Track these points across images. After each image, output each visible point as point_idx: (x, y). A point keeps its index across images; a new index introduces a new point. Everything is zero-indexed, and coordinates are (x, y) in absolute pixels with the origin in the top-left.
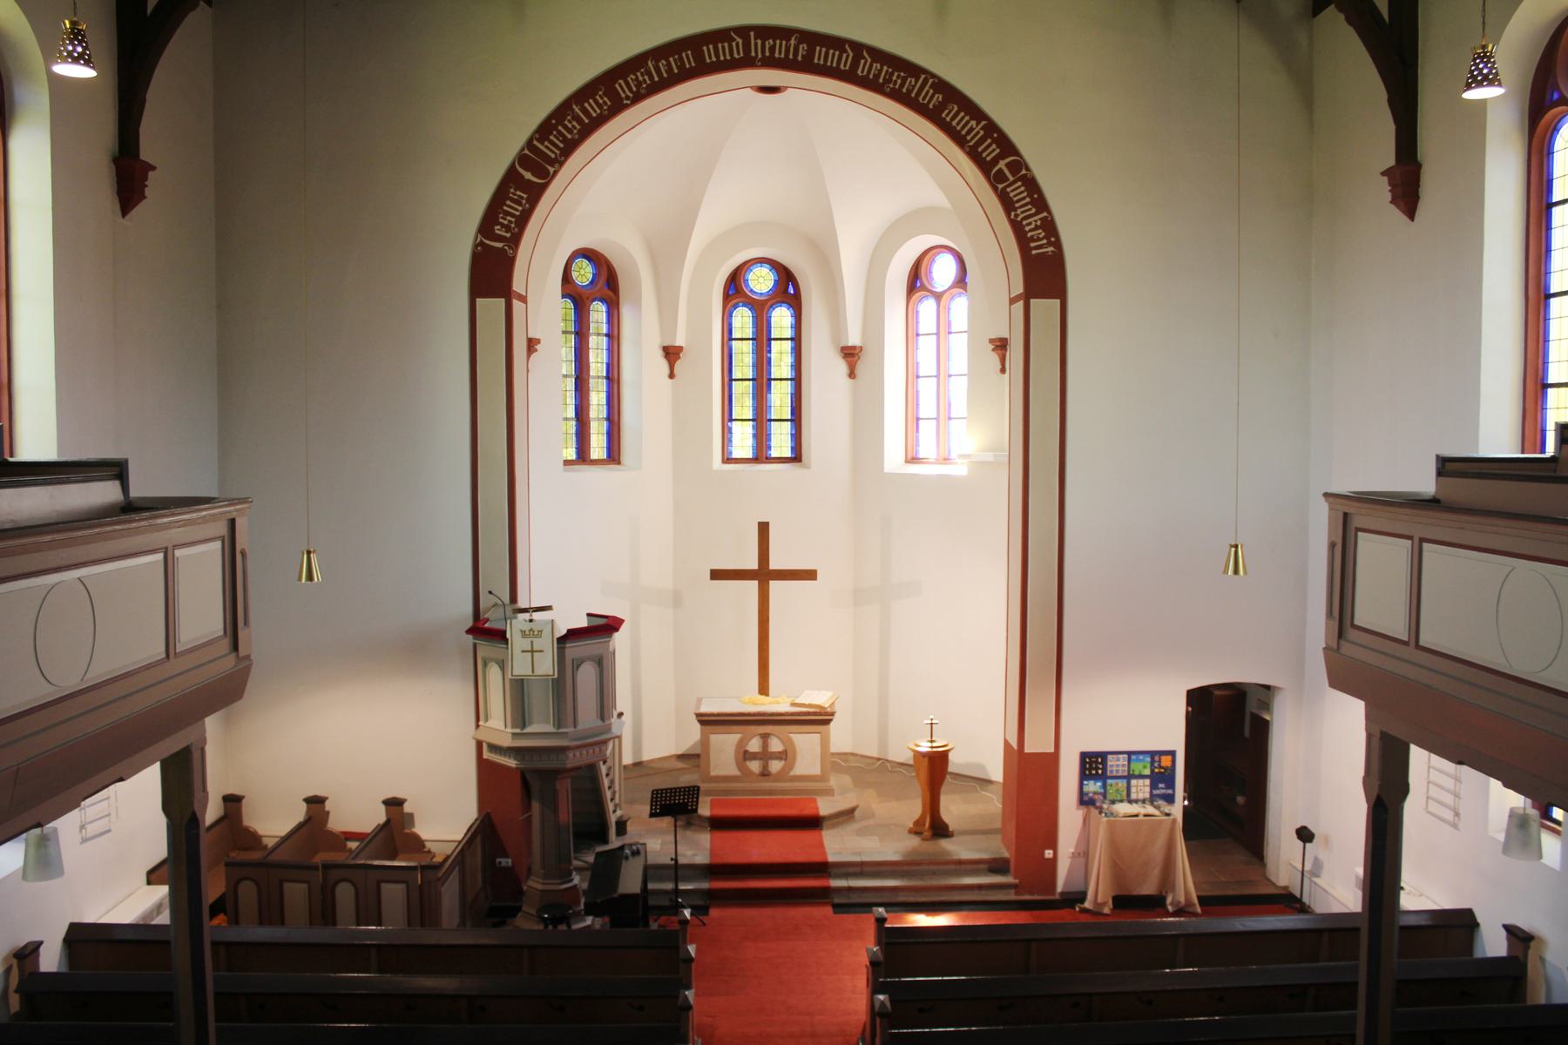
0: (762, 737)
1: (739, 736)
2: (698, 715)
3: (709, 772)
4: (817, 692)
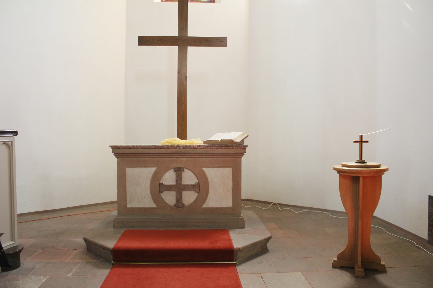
0: (175, 171)
1: (154, 169)
2: (112, 147)
3: (126, 205)
4: (229, 133)
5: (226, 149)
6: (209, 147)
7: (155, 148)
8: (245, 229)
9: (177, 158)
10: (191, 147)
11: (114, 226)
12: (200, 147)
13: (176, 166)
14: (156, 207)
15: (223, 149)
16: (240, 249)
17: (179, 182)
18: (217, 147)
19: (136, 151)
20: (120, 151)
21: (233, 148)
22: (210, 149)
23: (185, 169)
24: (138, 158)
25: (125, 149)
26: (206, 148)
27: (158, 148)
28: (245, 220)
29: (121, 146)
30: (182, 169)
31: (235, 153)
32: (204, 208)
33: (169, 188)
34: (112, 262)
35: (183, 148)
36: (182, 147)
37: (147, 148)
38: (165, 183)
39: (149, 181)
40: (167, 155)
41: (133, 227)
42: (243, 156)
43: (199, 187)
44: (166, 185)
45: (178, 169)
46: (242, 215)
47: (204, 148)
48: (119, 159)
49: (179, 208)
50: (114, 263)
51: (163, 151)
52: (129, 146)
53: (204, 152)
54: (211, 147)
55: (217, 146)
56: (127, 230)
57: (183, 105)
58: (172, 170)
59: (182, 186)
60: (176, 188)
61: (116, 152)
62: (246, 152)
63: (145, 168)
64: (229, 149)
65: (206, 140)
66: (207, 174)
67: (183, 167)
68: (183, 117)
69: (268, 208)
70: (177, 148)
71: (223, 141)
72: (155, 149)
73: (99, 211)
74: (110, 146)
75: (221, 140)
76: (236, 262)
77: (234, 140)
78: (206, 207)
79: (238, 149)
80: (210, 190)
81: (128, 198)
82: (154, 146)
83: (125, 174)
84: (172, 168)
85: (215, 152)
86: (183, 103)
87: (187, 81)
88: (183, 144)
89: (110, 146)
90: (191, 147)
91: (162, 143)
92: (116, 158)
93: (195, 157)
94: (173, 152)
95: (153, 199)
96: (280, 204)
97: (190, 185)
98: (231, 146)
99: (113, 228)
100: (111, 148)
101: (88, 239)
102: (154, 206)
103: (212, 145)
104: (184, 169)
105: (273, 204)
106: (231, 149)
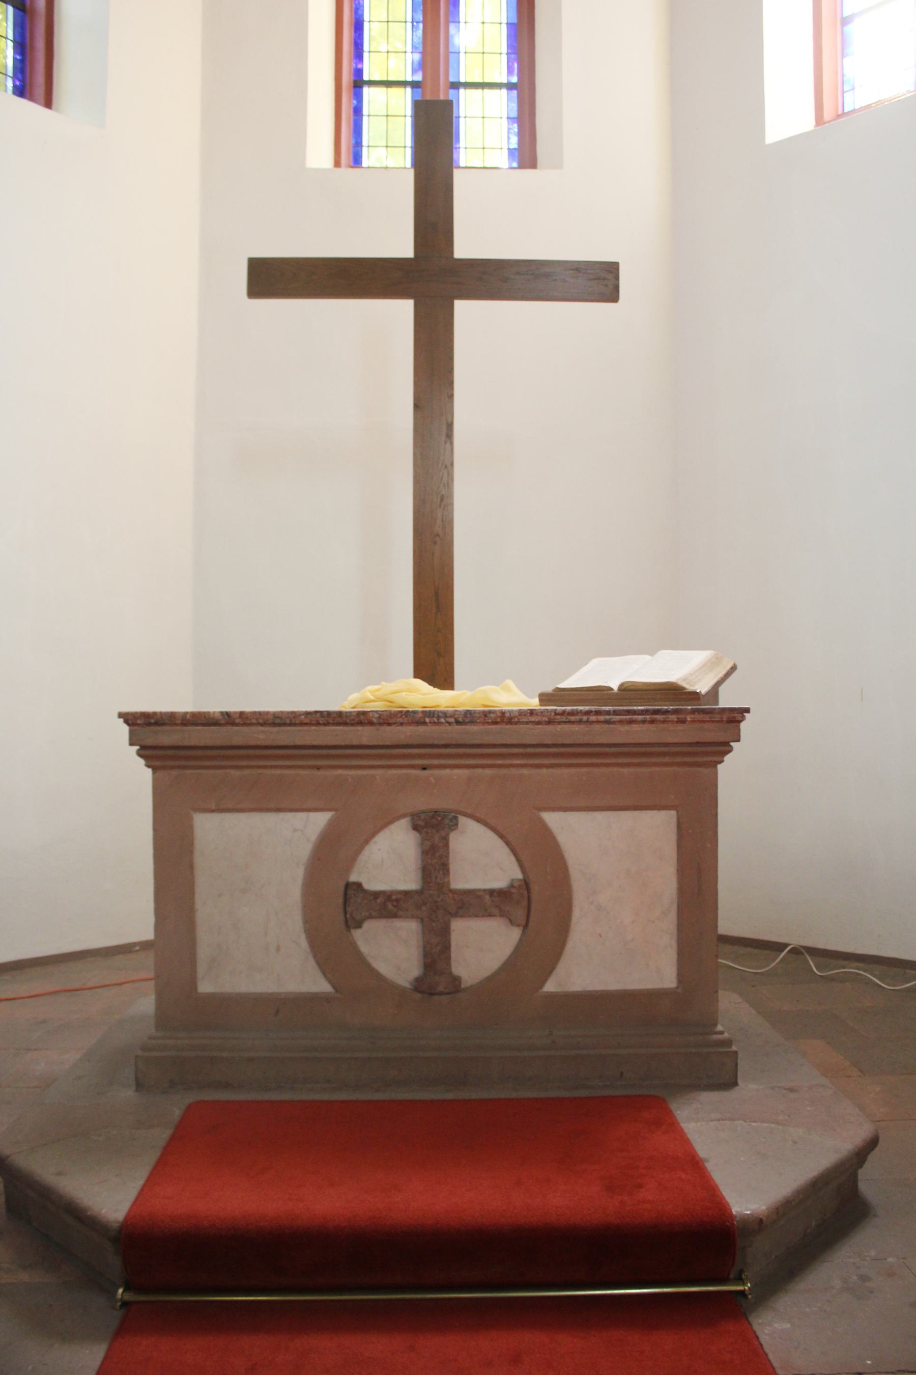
0: (416, 828)
1: (319, 820)
4: (648, 657)
5: (652, 727)
6: (572, 718)
7: (325, 725)
8: (733, 1094)
9: (425, 769)
10: (492, 715)
11: (137, 1079)
12: (533, 719)
13: (423, 802)
14: (331, 993)
15: (635, 727)
16: (761, 1220)
17: (436, 878)
18: (608, 717)
19: (239, 735)
20: (168, 737)
21: (683, 721)
22: (576, 728)
23: (462, 820)
24: (247, 767)
25: (190, 728)
26: (560, 723)
27: (340, 720)
28: (734, 1048)
29: (172, 715)
30: (451, 820)
31: (691, 744)
32: (552, 996)
33: (390, 906)
34: (121, 1291)
35: (452, 720)
36: (451, 717)
37: (288, 722)
38: (373, 884)
39: (300, 873)
40: (380, 757)
41: (227, 1086)
42: (727, 758)
43: (525, 903)
44: (376, 895)
45: (433, 817)
46: (719, 1028)
47: (549, 722)
48: (161, 774)
49: (436, 998)
50: (129, 1297)
51: (365, 735)
52: (209, 713)
53: (550, 742)
54: (585, 718)
55: (608, 713)
56: (199, 1102)
57: (435, 543)
58: (404, 823)
59: (451, 895)
60: (424, 908)
61: (149, 742)
62: (739, 741)
63: (282, 815)
64: (665, 725)
65: (549, 689)
66: (562, 839)
67: (451, 811)
68: (437, 594)
69: (765, 971)
70: (427, 720)
71: (630, 691)
72: (327, 728)
73: (90, 985)
74: (121, 715)
75: (623, 688)
76: (741, 1288)
77: (684, 685)
78: (559, 990)
79: (706, 726)
80: (576, 913)
81: (204, 952)
82: (321, 712)
83: (192, 844)
84: (403, 816)
85: (601, 741)
86: (438, 535)
87: (452, 444)
88: (444, 706)
89: (121, 715)
90: (492, 715)
91: (353, 706)
92: (149, 771)
93: (508, 762)
94: (410, 742)
95: (314, 957)
96: (813, 952)
97: (484, 890)
98: (675, 712)
99: (134, 1088)
100: (126, 722)
101: (8, 1157)
102: (323, 986)
103: (587, 708)
104: (456, 818)
105: (790, 951)
106: (671, 727)
